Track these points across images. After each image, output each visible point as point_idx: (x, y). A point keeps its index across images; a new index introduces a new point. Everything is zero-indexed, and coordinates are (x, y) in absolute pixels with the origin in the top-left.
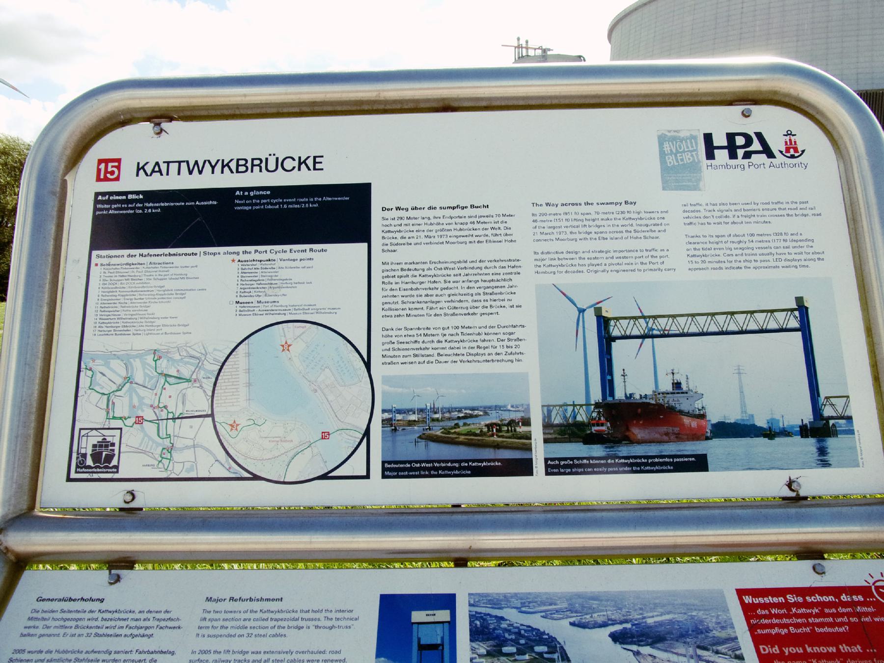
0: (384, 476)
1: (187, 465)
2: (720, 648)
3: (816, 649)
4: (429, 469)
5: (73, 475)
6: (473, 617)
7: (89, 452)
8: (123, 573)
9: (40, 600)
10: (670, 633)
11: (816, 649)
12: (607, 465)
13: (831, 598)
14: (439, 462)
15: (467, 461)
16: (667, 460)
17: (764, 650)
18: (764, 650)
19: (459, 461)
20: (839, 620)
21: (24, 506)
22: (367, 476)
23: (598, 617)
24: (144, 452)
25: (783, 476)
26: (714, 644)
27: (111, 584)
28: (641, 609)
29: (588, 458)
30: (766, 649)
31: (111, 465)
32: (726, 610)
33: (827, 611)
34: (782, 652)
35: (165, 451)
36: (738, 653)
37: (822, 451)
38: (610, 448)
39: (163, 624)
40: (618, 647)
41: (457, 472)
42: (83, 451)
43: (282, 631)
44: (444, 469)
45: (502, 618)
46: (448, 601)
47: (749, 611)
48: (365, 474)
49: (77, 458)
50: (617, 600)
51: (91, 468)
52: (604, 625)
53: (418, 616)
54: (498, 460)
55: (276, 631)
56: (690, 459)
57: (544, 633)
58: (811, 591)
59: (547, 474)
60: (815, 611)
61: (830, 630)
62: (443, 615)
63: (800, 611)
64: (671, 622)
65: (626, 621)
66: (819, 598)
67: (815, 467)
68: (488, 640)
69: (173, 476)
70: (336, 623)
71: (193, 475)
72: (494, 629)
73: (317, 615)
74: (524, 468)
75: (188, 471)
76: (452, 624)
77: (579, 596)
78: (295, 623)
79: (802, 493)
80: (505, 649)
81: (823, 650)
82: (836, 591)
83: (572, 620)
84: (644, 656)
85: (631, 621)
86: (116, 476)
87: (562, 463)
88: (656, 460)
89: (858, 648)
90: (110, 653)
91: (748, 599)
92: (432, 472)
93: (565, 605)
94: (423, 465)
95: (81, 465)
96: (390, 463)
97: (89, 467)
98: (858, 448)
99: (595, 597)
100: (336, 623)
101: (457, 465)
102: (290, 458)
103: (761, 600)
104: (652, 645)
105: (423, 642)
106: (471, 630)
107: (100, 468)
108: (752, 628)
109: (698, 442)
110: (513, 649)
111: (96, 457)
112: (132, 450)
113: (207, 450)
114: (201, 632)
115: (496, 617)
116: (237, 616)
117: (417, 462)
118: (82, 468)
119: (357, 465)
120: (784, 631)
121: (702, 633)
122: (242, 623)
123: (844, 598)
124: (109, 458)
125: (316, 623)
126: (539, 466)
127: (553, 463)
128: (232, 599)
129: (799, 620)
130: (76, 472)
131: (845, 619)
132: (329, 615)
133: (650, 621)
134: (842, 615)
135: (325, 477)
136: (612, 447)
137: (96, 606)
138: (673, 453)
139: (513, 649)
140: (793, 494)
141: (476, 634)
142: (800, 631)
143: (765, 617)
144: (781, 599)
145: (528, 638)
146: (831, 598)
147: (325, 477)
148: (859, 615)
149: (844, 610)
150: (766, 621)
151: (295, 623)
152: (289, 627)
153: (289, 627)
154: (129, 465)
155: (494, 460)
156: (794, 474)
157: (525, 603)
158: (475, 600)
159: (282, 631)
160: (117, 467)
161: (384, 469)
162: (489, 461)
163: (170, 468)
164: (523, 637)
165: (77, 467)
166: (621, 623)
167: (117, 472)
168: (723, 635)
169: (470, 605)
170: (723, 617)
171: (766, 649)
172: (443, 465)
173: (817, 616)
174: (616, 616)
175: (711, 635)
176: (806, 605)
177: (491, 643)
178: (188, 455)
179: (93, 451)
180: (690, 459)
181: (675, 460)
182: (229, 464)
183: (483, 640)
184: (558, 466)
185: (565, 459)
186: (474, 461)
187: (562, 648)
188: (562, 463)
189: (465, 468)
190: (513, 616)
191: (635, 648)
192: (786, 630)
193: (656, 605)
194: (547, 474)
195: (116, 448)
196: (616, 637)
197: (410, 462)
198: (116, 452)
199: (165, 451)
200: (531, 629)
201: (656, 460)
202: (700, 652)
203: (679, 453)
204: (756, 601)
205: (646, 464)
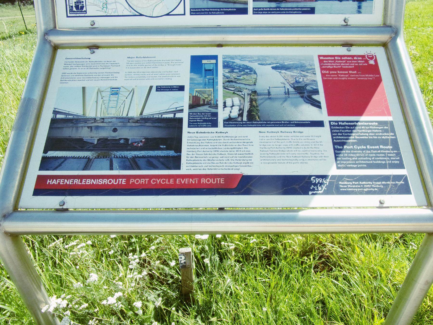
0: (191, 14)
1: (114, 10)
2: (308, 71)
3: (341, 72)
4: (208, 12)
5: (69, 15)
6: (224, 62)
7: (74, 5)
8: (95, 50)
9: (67, 59)
10: (292, 67)
11: (341, 72)
12: (276, 11)
13: (350, 58)
14: (212, 9)
15: (223, 8)
16: (299, 9)
17: (332, 123)
18: (332, 123)
19: (220, 8)
20: (352, 64)
21: (52, 26)
22: (184, 14)
23: (268, 62)
24: (96, 5)
25: (343, 17)
26: (306, 70)
27: (92, 53)
28: (283, 60)
29: (269, 8)
30: (324, 72)
31: (83, 10)
32: (313, 61)
33: (348, 62)
34: (329, 73)
35: (104, 4)
36: (314, 73)
37: (359, 7)
38: (278, 4)
39: (113, 65)
40: (274, 70)
41: (219, 13)
42: (71, 5)
43: (156, 66)
44: (214, 11)
45: (234, 62)
46: (215, 57)
47: (321, 61)
48: (183, 13)
49: (69, 8)
50: (275, 58)
51: (76, 12)
52: (270, 64)
53: (204, 62)
54: (235, 8)
55: (154, 66)
56: (309, 9)
57: (248, 66)
58: (344, 56)
59: (253, 14)
60: (344, 61)
61: (347, 67)
62: (214, 61)
63: (338, 62)
64: (293, 64)
65: (278, 63)
66: (346, 58)
67: (356, 14)
68: (229, 68)
69: (108, 15)
70: (176, 64)
71: (116, 14)
72: (231, 65)
73: (169, 62)
74: (244, 11)
75: (114, 12)
76: (216, 64)
77: (262, 56)
78: (161, 64)
79: (349, 24)
80: (235, 71)
81: (344, 72)
82: (353, 56)
83: (259, 63)
84: (282, 73)
85: (279, 63)
86: (86, 15)
87: (259, 10)
88: (296, 9)
89: (356, 72)
90: (97, 73)
91: (321, 58)
92: (210, 13)
93: (257, 59)
94: (206, 10)
95: (71, 11)
96: (193, 9)
97: (75, 11)
98: (374, 7)
99: (267, 56)
100: (176, 64)
101: (219, 10)
102: (154, 7)
103: (326, 58)
104: (285, 70)
105: (206, 69)
106: (223, 66)
107: (79, 12)
108: (321, 66)
109: (312, 2)
110: (238, 71)
111: (77, 7)
112: (92, 4)
113: (121, 4)
114: (127, 67)
115: (232, 62)
116: (140, 62)
117: (204, 9)
118: (72, 12)
119: (180, 10)
120: (331, 67)
121: (303, 67)
122: (142, 64)
123: (355, 58)
124: (82, 8)
125: (168, 64)
126: (250, 11)
127: (256, 10)
128: (137, 57)
129: (338, 64)
130: (70, 14)
131: (354, 64)
132: (173, 62)
133: (286, 63)
134: (353, 63)
135: (168, 14)
136: (279, 3)
137: (88, 60)
138: (302, 7)
139: (238, 71)
140: (345, 24)
141: (225, 67)
142: (337, 67)
143: (326, 63)
144: (333, 58)
145: (243, 68)
146: (350, 58)
147: (168, 14)
148: (359, 63)
149: (354, 62)
150: (326, 64)
151: (161, 64)
152: (159, 65)
153: (159, 65)
154: (90, 10)
155: (233, 8)
156: (347, 16)
157: (242, 58)
158: (225, 57)
159: (156, 66)
160: (86, 11)
161: (191, 12)
162: (231, 8)
163: (107, 11)
164: (241, 67)
165: (70, 11)
166: (276, 64)
167: (86, 13)
168: (310, 68)
169: (223, 58)
170: (311, 63)
171: (324, 72)
172: (213, 10)
173: (344, 63)
174: (274, 62)
175: (306, 67)
176: (341, 60)
177: (230, 69)
178: (113, 6)
179: (75, 4)
180: (309, 9)
181: (303, 9)
182: (130, 9)
183: (227, 68)
184: (258, 11)
185: (260, 8)
186: (225, 8)
187: (254, 71)
188: (259, 10)
189: (222, 11)
190: (238, 62)
191: (279, 71)
192: (332, 67)
193: (289, 59)
194: (253, 14)
195: (84, 3)
196: (273, 68)
197: (201, 9)
198: (84, 5)
199: (104, 4)
200: (244, 65)
201: (296, 9)
202: (301, 72)
203: (305, 7)
204: (324, 58)
205: (291, 11)
